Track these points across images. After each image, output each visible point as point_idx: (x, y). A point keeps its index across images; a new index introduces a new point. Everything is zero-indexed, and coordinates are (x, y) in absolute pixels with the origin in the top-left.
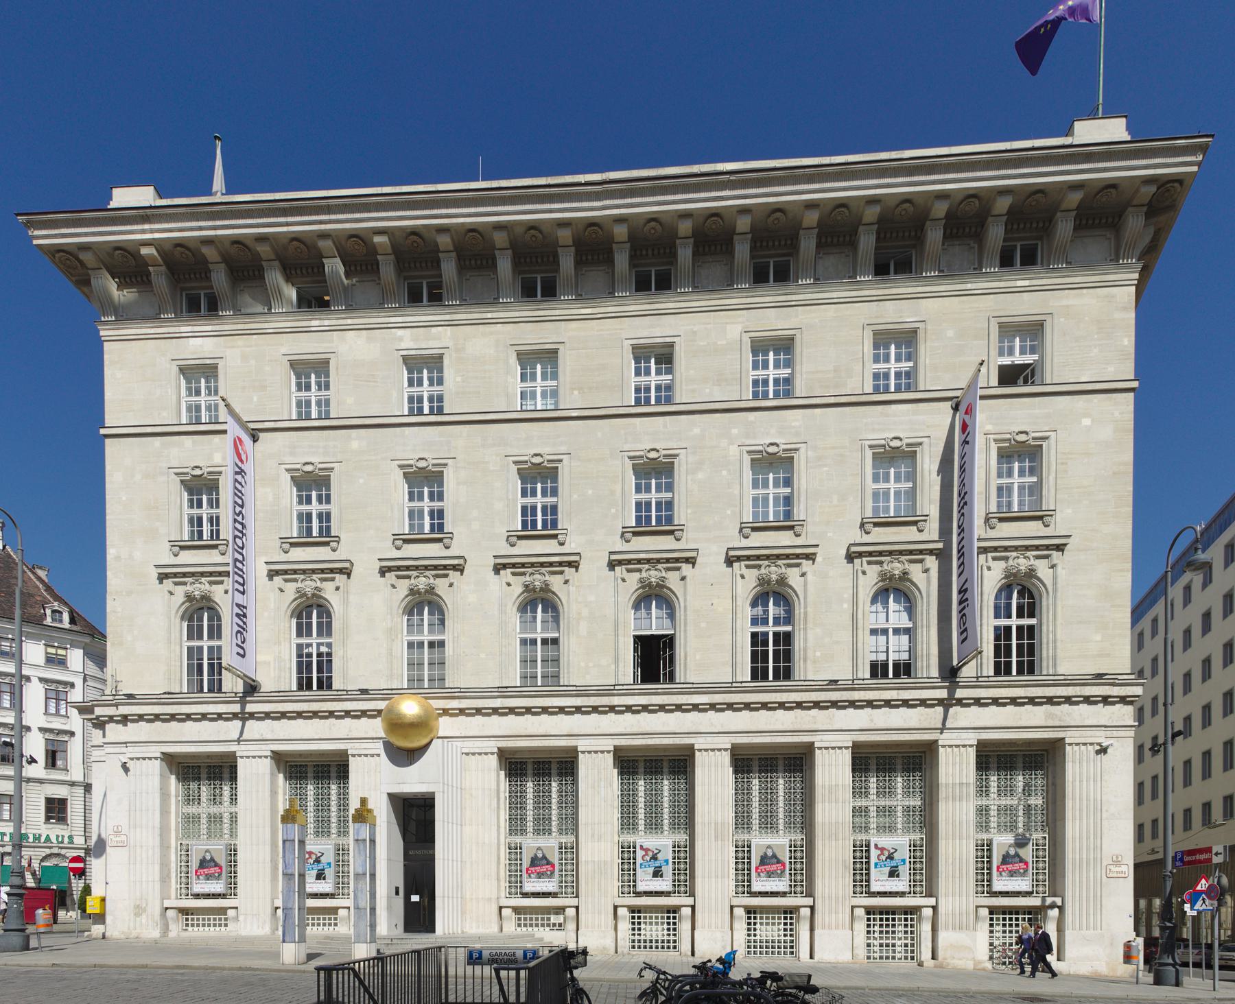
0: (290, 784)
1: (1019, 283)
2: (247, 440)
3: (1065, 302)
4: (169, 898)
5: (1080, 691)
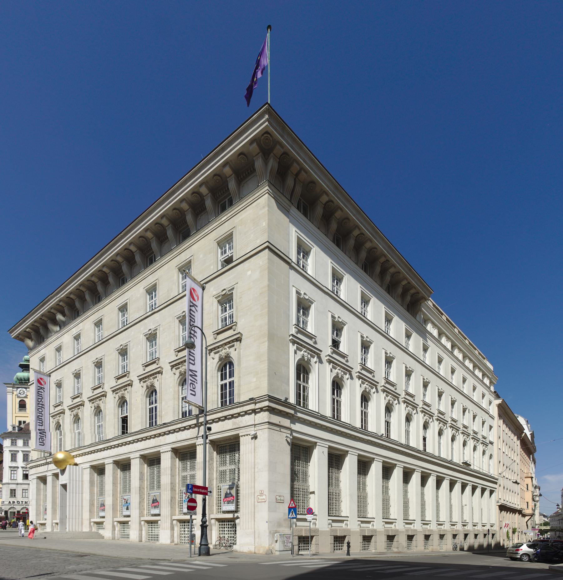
0: (219, 456)
1: (223, 219)
2: (199, 290)
3: (240, 218)
4: (175, 515)
5: (242, 409)
